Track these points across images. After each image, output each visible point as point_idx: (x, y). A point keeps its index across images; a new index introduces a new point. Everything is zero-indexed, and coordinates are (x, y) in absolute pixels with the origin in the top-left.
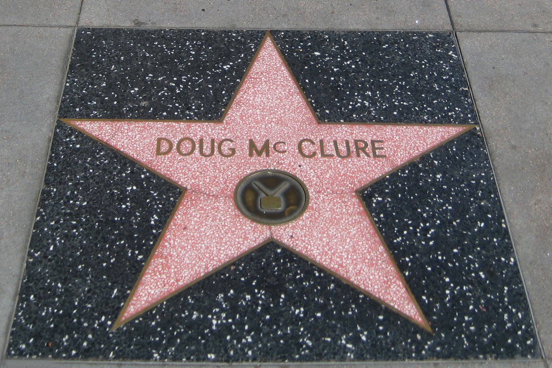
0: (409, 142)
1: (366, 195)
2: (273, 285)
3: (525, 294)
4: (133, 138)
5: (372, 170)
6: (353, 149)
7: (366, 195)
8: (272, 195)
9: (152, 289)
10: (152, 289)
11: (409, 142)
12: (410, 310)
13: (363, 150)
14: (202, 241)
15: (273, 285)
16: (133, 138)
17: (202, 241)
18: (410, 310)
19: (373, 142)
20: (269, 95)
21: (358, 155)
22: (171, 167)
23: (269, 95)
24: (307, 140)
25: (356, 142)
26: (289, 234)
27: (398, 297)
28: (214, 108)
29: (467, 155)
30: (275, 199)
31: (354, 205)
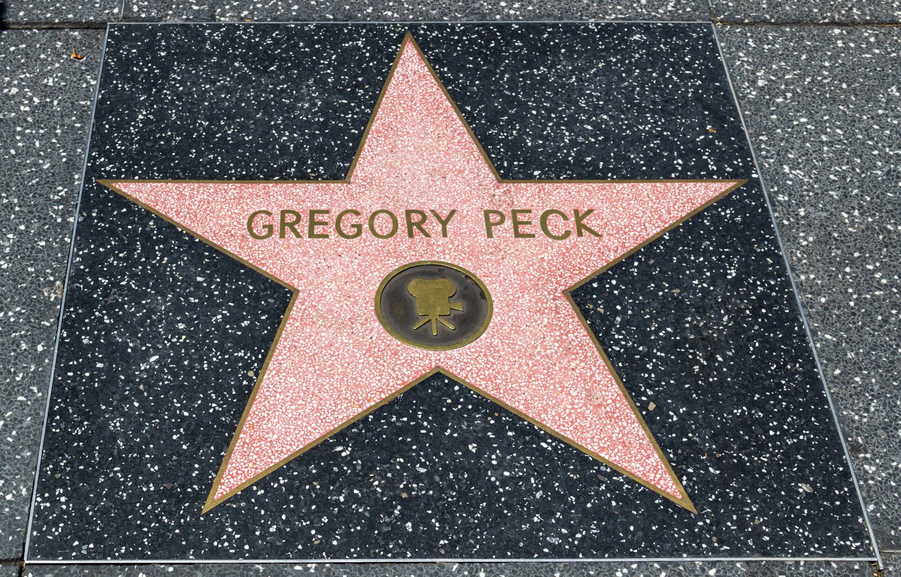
0: (639, 211)
1: (581, 296)
2: (433, 453)
3: (181, 559)
4: (211, 210)
5: (591, 257)
6: (402, 228)
7: (581, 296)
8: (432, 301)
9: (243, 466)
10: (243, 466)
11: (639, 211)
12: (669, 485)
13: (291, 226)
14: (319, 381)
15: (433, 453)
16: (211, 210)
17: (319, 381)
18: (669, 485)
19: (514, 213)
20: (418, 139)
21: (282, 235)
22: (272, 258)
23: (418, 139)
24: (383, 211)
25: (409, 213)
26: (463, 362)
27: (646, 464)
28: (334, 156)
29: (738, 232)
30: (434, 304)
31: (567, 307)
